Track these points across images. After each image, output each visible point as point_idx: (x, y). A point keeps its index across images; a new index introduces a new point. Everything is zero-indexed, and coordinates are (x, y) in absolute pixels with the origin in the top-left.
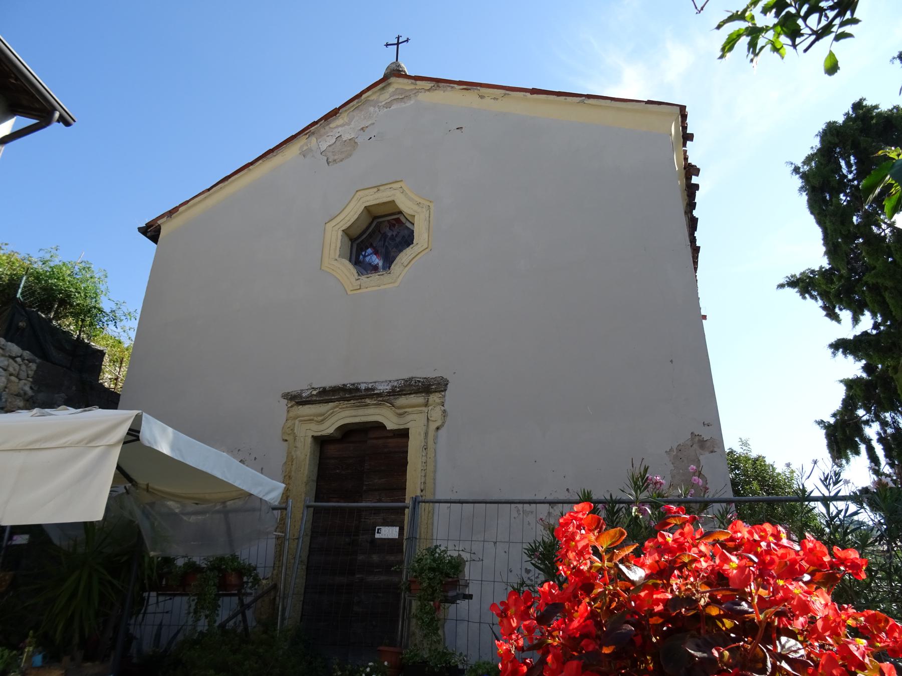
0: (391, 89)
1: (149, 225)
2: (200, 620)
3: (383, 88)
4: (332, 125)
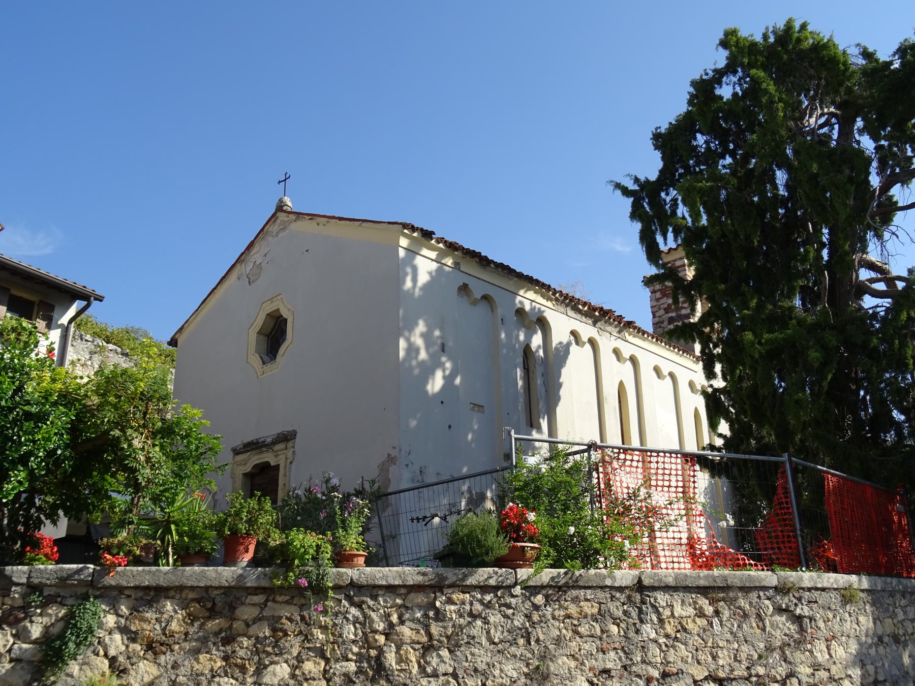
0: (279, 221)
1: (172, 339)
2: (110, 667)
3: (275, 221)
4: (252, 254)
